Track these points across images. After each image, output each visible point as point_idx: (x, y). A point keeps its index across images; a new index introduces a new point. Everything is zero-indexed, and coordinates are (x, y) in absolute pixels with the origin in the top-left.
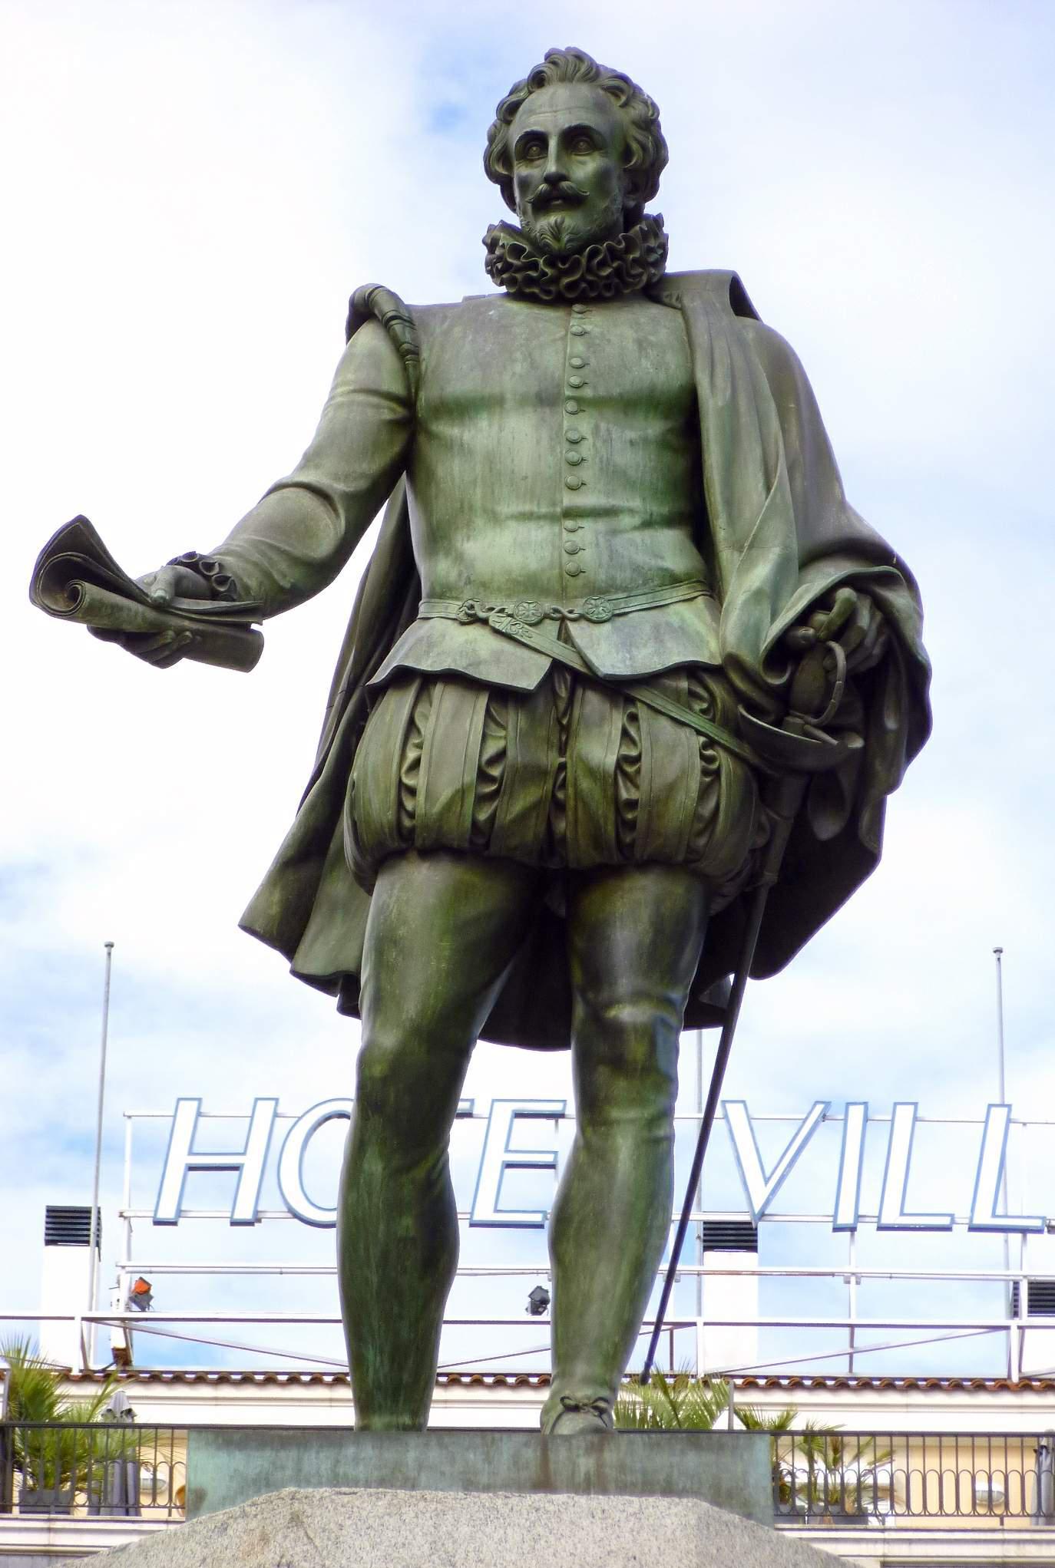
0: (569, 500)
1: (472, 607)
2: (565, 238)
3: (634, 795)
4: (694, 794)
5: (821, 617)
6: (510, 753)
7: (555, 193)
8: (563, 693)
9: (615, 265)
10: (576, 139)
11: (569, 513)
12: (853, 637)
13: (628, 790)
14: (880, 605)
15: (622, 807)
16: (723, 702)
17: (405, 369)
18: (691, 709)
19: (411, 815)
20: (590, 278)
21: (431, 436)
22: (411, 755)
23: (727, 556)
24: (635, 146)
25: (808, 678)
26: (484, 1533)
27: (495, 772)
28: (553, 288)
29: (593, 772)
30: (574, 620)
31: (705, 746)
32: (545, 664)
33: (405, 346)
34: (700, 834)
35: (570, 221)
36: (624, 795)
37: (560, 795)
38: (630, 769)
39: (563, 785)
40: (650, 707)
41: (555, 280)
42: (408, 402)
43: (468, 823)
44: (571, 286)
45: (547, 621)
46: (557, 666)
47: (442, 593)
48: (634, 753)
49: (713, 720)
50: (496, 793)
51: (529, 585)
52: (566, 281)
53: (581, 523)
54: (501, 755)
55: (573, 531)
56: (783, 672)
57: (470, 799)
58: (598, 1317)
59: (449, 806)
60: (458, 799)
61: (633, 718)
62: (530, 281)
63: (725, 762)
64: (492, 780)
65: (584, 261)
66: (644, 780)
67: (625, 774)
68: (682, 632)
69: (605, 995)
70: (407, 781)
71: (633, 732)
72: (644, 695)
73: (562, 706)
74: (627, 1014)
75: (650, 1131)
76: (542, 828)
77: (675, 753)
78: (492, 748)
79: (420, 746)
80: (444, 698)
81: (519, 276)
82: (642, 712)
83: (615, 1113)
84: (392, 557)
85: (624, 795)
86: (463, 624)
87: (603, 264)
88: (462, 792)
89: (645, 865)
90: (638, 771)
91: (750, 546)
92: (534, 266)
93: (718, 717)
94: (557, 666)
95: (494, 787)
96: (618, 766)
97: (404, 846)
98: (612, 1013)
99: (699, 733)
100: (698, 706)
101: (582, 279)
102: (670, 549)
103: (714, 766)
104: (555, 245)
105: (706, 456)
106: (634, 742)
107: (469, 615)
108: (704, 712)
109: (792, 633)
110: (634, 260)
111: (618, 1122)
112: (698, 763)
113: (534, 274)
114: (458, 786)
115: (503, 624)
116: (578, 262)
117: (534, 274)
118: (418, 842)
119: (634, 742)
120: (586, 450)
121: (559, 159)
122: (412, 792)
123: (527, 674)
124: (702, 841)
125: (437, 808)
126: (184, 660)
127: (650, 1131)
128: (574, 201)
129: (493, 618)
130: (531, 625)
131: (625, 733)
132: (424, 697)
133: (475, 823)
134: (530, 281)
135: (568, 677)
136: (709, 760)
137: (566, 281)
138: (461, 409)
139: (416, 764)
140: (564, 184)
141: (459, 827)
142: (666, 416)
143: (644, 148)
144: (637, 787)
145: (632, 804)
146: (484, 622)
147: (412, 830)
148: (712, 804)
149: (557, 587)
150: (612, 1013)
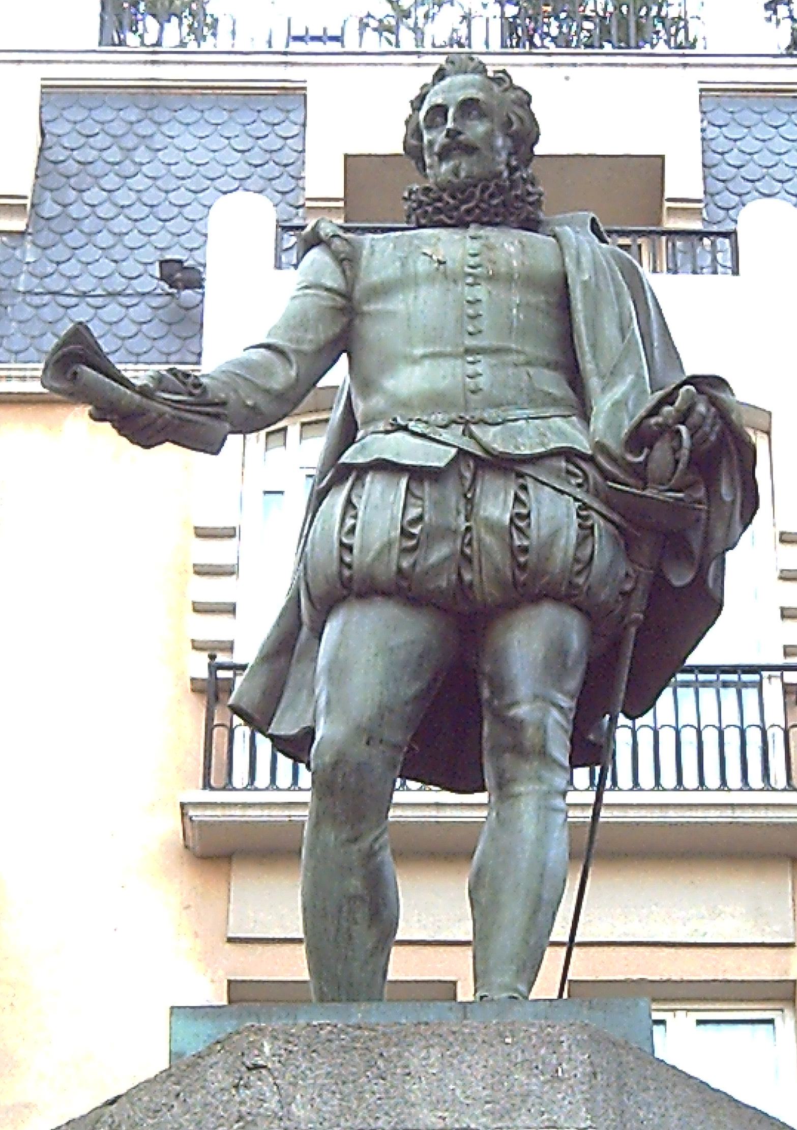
0: (470, 342)
1: (395, 419)
2: (463, 174)
3: (526, 543)
4: (573, 540)
5: (667, 409)
6: (426, 518)
7: (454, 145)
8: (468, 475)
9: (502, 197)
10: (468, 107)
11: (468, 351)
12: (694, 419)
13: (520, 539)
14: (713, 402)
15: (515, 552)
16: (595, 479)
17: (344, 272)
18: (569, 483)
19: (349, 566)
20: (483, 205)
21: (363, 314)
22: (349, 522)
23: (594, 383)
24: (514, 118)
25: (661, 452)
26: (409, 1051)
27: (416, 530)
28: (455, 214)
29: (492, 526)
30: (474, 423)
31: (579, 507)
32: (454, 451)
33: (342, 256)
34: (579, 573)
35: (466, 166)
36: (517, 542)
37: (468, 551)
38: (522, 524)
39: (470, 544)
40: (536, 479)
41: (457, 208)
42: (347, 296)
43: (394, 568)
44: (469, 212)
45: (454, 425)
46: (461, 452)
47: (370, 420)
48: (524, 511)
49: (587, 491)
50: (414, 549)
51: (435, 400)
52: (464, 207)
53: (479, 357)
54: (420, 518)
55: (473, 363)
56: (641, 453)
57: (395, 551)
58: (508, 940)
59: (380, 553)
60: (386, 551)
61: (524, 488)
62: (439, 211)
63: (598, 522)
64: (413, 536)
65: (478, 193)
66: (533, 532)
67: (519, 529)
68: (561, 433)
69: (507, 699)
70: (345, 540)
71: (523, 496)
72: (527, 470)
73: (467, 484)
74: (523, 711)
75: (546, 800)
76: (454, 577)
77: (554, 513)
78: (413, 513)
79: (355, 517)
80: (374, 484)
81: (430, 209)
82: (530, 483)
83: (520, 788)
84: (391, 894)
85: (517, 542)
86: (387, 432)
87: (492, 196)
88: (389, 544)
89: (537, 599)
90: (529, 525)
91: (612, 375)
92: (440, 199)
93: (591, 489)
94: (461, 452)
95: (414, 542)
96: (511, 520)
97: (345, 592)
98: (513, 712)
99: (576, 499)
100: (574, 481)
101: (477, 206)
102: (552, 383)
103: (589, 523)
104: (455, 180)
105: (573, 303)
106: (524, 504)
107: (392, 425)
108: (579, 485)
109: (643, 426)
110: (517, 196)
111: (520, 794)
112: (575, 520)
113: (439, 205)
114: (386, 539)
115: (420, 428)
116: (472, 195)
117: (439, 205)
118: (355, 587)
119: (524, 504)
120: (482, 309)
121: (455, 120)
122: (350, 548)
123: (437, 456)
124: (580, 580)
125: (368, 559)
126: (168, 445)
127: (546, 800)
128: (469, 149)
129: (411, 425)
130: (441, 427)
131: (517, 498)
132: (359, 483)
133: (400, 570)
134: (439, 211)
135: (472, 464)
136: (586, 518)
137: (464, 207)
138: (383, 290)
139: (353, 529)
140: (462, 137)
141: (385, 572)
142: (546, 293)
143: (521, 119)
144: (527, 537)
145: (525, 550)
146: (405, 429)
147: (350, 578)
148: (588, 551)
149: (462, 400)
150: (513, 712)
